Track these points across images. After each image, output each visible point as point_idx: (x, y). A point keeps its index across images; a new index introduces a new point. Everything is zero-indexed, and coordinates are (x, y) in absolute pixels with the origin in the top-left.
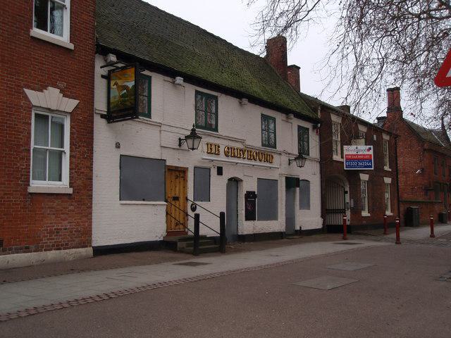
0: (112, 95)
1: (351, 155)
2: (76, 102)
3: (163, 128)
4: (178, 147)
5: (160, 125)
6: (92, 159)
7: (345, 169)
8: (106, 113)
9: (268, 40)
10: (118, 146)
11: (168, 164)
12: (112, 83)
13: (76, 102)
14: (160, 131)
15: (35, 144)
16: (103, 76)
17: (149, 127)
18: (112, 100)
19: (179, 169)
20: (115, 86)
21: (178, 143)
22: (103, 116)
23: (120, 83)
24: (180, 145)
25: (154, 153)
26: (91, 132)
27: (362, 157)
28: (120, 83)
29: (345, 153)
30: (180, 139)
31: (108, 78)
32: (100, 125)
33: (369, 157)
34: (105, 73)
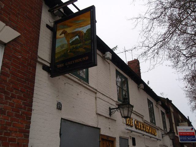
0: (58, 44)
1: (182, 133)
2: (16, 34)
3: (99, 95)
4: (108, 116)
5: (95, 91)
6: (30, 119)
7: (180, 142)
8: (49, 65)
9: (128, 62)
10: (59, 107)
11: (103, 132)
12: (58, 33)
13: (16, 34)
14: (96, 98)
15: (2, 135)
16: (48, 26)
17: (88, 92)
18: (57, 50)
19: (110, 139)
20: (63, 35)
21: (109, 112)
22: (45, 68)
23: (69, 30)
24: (110, 114)
25: (92, 122)
26: (32, 81)
27: (189, 134)
28: (69, 30)
29: (179, 131)
30: (110, 109)
31: (53, 30)
32: (41, 76)
33: (192, 134)
34: (51, 24)
